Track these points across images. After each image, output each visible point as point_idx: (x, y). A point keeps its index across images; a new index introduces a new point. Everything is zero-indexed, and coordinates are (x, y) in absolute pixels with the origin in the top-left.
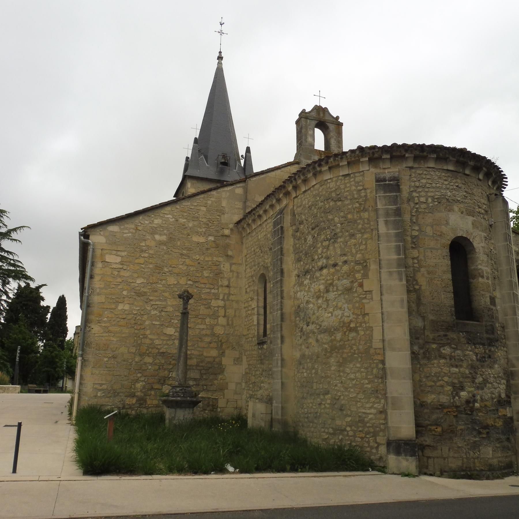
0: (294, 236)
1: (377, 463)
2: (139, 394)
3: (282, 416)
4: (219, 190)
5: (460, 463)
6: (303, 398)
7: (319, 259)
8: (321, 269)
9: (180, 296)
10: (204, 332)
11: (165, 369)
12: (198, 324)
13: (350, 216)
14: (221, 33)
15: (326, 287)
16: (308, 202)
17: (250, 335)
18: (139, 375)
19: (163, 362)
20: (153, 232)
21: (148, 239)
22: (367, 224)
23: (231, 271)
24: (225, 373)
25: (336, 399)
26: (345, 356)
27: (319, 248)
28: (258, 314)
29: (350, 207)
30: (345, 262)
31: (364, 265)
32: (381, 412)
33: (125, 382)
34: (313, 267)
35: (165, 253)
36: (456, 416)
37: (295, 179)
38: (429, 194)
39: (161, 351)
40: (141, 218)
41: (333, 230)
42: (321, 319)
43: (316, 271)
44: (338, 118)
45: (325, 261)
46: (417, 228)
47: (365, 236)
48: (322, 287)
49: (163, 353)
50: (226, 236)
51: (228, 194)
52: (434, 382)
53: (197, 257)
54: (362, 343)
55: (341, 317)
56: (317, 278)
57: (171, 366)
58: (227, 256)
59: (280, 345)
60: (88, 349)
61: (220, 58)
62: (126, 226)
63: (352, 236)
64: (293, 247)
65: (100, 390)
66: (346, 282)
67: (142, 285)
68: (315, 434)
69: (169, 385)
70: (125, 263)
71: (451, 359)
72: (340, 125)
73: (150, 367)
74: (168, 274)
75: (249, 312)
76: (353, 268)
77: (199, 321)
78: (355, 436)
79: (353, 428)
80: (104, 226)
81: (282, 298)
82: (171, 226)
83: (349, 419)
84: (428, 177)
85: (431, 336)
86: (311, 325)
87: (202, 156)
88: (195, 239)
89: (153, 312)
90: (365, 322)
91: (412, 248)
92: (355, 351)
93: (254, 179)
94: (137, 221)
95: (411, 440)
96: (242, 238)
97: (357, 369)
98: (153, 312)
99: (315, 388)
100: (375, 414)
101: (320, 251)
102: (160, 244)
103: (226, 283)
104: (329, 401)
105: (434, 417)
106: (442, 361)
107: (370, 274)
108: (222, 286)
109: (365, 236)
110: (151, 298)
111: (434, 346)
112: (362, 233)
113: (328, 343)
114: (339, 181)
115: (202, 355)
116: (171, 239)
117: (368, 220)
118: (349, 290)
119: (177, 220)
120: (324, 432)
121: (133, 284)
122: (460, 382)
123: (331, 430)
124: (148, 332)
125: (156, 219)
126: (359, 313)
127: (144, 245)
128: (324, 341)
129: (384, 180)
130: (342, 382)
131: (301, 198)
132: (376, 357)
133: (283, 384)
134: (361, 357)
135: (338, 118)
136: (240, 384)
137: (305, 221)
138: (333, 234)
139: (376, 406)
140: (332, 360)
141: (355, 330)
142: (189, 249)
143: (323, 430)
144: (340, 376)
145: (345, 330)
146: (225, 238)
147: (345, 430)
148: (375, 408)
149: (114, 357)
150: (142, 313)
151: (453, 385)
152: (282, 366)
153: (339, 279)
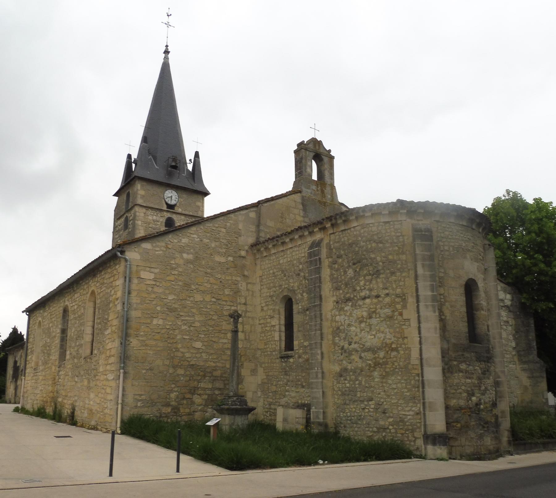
0: (330, 267)
1: (415, 452)
2: (173, 403)
3: (324, 419)
4: (236, 213)
5: (472, 450)
6: (345, 404)
7: (361, 290)
8: (364, 298)
9: (231, 316)
10: (226, 346)
11: (194, 380)
12: (221, 338)
13: (390, 257)
14: (168, 24)
15: (369, 314)
16: (348, 240)
17: (268, 349)
18: (173, 386)
19: (193, 373)
20: (182, 250)
21: (177, 257)
22: (405, 264)
23: (248, 290)
24: (244, 383)
25: (378, 405)
26: (387, 370)
27: (361, 281)
28: (280, 331)
29: (390, 249)
30: (387, 295)
31: (403, 298)
32: (417, 414)
33: (162, 393)
34: (355, 296)
35: (192, 272)
36: (469, 415)
37: (336, 219)
38: (452, 244)
39: (191, 363)
40: (170, 236)
41: (375, 267)
42: (364, 340)
43: (358, 299)
44: (330, 151)
45: (368, 292)
46: (442, 271)
47: (404, 275)
48: (365, 314)
49: (193, 365)
50: (244, 257)
51: (244, 217)
52: (455, 390)
53: (219, 276)
54: (402, 360)
55: (384, 339)
56: (360, 306)
57: (200, 378)
58: (244, 276)
59: (320, 360)
60: (128, 361)
61: (167, 52)
62: (158, 244)
63: (393, 273)
64: (330, 276)
65: (139, 401)
66: (388, 311)
67: (174, 302)
68: (359, 433)
69: (198, 395)
70: (158, 280)
71: (466, 373)
72: (332, 158)
73: (182, 378)
74: (195, 291)
75: (268, 329)
76: (394, 300)
77: (222, 335)
78: (396, 433)
79: (395, 426)
80: (139, 243)
81: (321, 320)
82: (196, 246)
83: (391, 420)
84: (450, 230)
85: (453, 355)
86: (353, 344)
87: (151, 157)
88: (218, 258)
89: (184, 327)
90: (404, 344)
91: (440, 286)
92: (396, 366)
93: (266, 205)
94: (167, 240)
95: (443, 434)
96: (255, 259)
97: (398, 381)
98: (184, 327)
99: (358, 396)
100: (413, 415)
101: (362, 283)
102: (187, 263)
103: (243, 301)
104: (373, 406)
105: (456, 416)
106: (461, 374)
107: (408, 305)
108: (240, 304)
109: (404, 275)
110: (181, 314)
111: (455, 363)
112: (400, 272)
113: (371, 360)
114: (381, 227)
115: (225, 366)
116: (197, 258)
117: (406, 261)
118: (391, 318)
119: (201, 241)
120: (368, 431)
121: (165, 300)
122: (472, 390)
123: (375, 429)
124: (179, 346)
125: (184, 238)
126: (400, 336)
127: (174, 262)
128: (369, 358)
129: (421, 231)
130: (385, 391)
131: (339, 235)
132: (413, 371)
133: (323, 392)
134: (401, 371)
135: (330, 151)
136: (256, 392)
137: (344, 256)
138: (375, 270)
139: (413, 409)
140: (376, 374)
141: (396, 349)
142: (212, 269)
143: (367, 429)
144: (382, 386)
145: (388, 350)
146: (241, 258)
147: (388, 428)
148: (413, 411)
149: (151, 369)
150: (174, 327)
151: (467, 392)
152: (323, 377)
153: (381, 308)
